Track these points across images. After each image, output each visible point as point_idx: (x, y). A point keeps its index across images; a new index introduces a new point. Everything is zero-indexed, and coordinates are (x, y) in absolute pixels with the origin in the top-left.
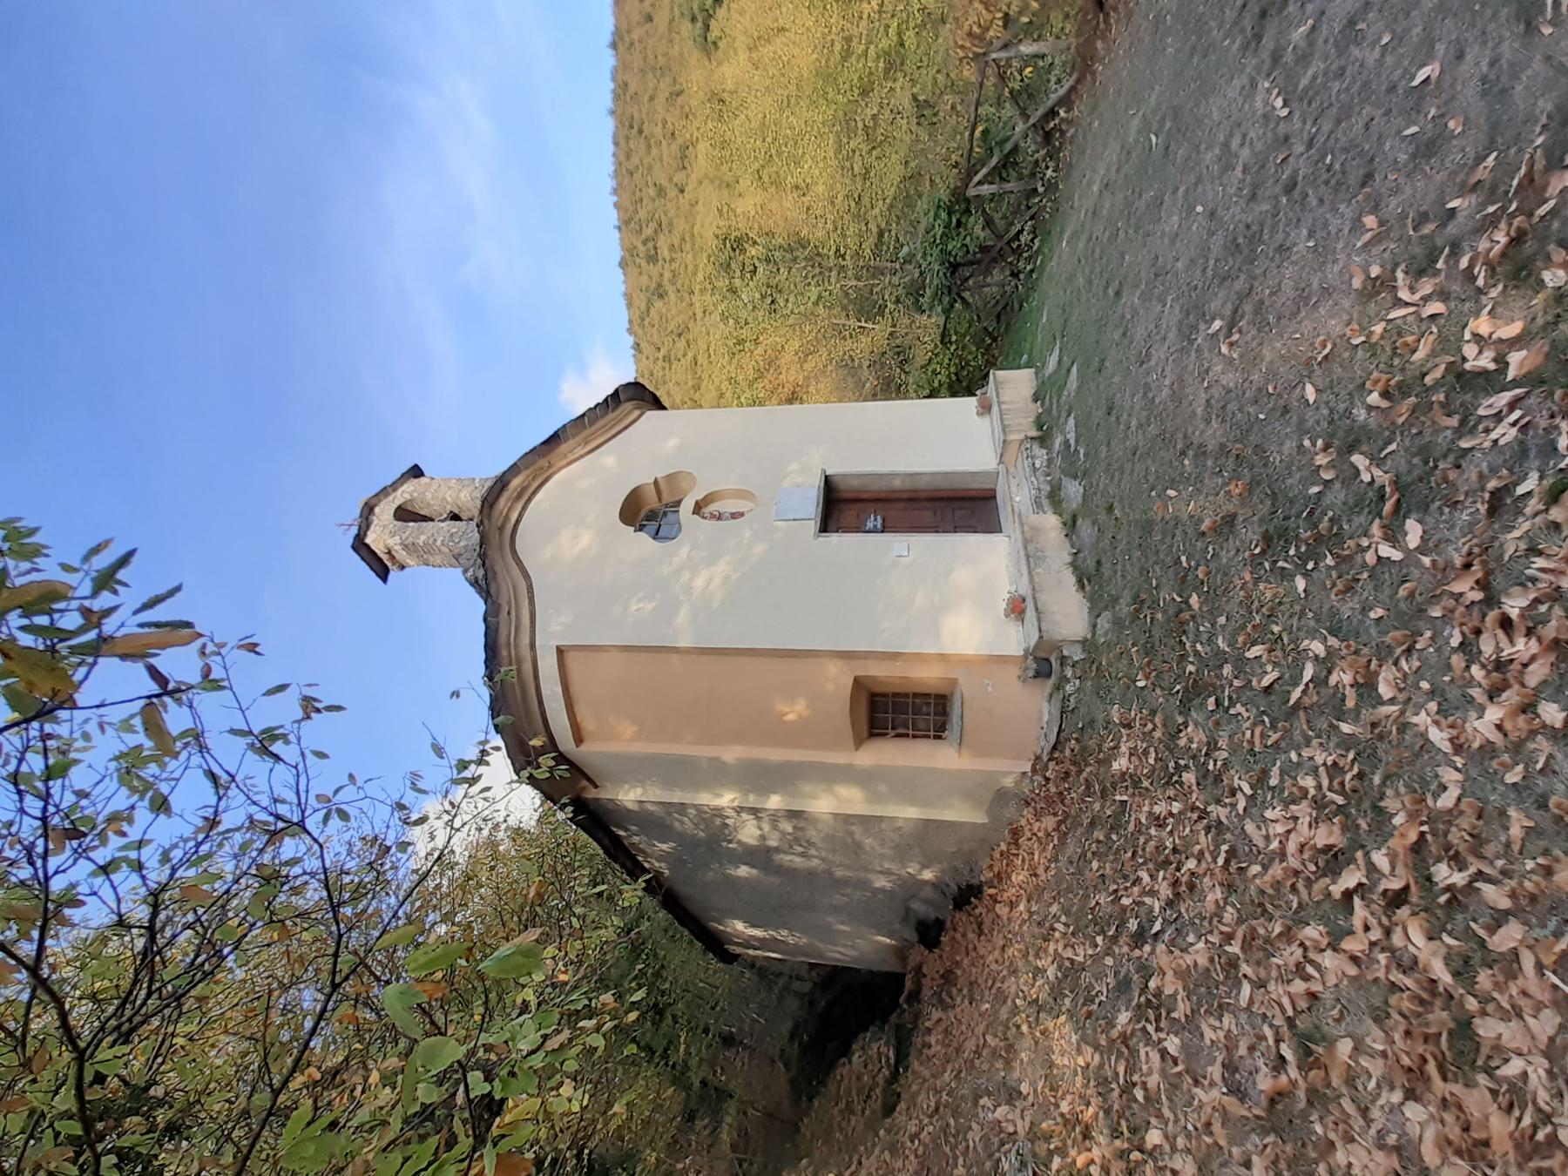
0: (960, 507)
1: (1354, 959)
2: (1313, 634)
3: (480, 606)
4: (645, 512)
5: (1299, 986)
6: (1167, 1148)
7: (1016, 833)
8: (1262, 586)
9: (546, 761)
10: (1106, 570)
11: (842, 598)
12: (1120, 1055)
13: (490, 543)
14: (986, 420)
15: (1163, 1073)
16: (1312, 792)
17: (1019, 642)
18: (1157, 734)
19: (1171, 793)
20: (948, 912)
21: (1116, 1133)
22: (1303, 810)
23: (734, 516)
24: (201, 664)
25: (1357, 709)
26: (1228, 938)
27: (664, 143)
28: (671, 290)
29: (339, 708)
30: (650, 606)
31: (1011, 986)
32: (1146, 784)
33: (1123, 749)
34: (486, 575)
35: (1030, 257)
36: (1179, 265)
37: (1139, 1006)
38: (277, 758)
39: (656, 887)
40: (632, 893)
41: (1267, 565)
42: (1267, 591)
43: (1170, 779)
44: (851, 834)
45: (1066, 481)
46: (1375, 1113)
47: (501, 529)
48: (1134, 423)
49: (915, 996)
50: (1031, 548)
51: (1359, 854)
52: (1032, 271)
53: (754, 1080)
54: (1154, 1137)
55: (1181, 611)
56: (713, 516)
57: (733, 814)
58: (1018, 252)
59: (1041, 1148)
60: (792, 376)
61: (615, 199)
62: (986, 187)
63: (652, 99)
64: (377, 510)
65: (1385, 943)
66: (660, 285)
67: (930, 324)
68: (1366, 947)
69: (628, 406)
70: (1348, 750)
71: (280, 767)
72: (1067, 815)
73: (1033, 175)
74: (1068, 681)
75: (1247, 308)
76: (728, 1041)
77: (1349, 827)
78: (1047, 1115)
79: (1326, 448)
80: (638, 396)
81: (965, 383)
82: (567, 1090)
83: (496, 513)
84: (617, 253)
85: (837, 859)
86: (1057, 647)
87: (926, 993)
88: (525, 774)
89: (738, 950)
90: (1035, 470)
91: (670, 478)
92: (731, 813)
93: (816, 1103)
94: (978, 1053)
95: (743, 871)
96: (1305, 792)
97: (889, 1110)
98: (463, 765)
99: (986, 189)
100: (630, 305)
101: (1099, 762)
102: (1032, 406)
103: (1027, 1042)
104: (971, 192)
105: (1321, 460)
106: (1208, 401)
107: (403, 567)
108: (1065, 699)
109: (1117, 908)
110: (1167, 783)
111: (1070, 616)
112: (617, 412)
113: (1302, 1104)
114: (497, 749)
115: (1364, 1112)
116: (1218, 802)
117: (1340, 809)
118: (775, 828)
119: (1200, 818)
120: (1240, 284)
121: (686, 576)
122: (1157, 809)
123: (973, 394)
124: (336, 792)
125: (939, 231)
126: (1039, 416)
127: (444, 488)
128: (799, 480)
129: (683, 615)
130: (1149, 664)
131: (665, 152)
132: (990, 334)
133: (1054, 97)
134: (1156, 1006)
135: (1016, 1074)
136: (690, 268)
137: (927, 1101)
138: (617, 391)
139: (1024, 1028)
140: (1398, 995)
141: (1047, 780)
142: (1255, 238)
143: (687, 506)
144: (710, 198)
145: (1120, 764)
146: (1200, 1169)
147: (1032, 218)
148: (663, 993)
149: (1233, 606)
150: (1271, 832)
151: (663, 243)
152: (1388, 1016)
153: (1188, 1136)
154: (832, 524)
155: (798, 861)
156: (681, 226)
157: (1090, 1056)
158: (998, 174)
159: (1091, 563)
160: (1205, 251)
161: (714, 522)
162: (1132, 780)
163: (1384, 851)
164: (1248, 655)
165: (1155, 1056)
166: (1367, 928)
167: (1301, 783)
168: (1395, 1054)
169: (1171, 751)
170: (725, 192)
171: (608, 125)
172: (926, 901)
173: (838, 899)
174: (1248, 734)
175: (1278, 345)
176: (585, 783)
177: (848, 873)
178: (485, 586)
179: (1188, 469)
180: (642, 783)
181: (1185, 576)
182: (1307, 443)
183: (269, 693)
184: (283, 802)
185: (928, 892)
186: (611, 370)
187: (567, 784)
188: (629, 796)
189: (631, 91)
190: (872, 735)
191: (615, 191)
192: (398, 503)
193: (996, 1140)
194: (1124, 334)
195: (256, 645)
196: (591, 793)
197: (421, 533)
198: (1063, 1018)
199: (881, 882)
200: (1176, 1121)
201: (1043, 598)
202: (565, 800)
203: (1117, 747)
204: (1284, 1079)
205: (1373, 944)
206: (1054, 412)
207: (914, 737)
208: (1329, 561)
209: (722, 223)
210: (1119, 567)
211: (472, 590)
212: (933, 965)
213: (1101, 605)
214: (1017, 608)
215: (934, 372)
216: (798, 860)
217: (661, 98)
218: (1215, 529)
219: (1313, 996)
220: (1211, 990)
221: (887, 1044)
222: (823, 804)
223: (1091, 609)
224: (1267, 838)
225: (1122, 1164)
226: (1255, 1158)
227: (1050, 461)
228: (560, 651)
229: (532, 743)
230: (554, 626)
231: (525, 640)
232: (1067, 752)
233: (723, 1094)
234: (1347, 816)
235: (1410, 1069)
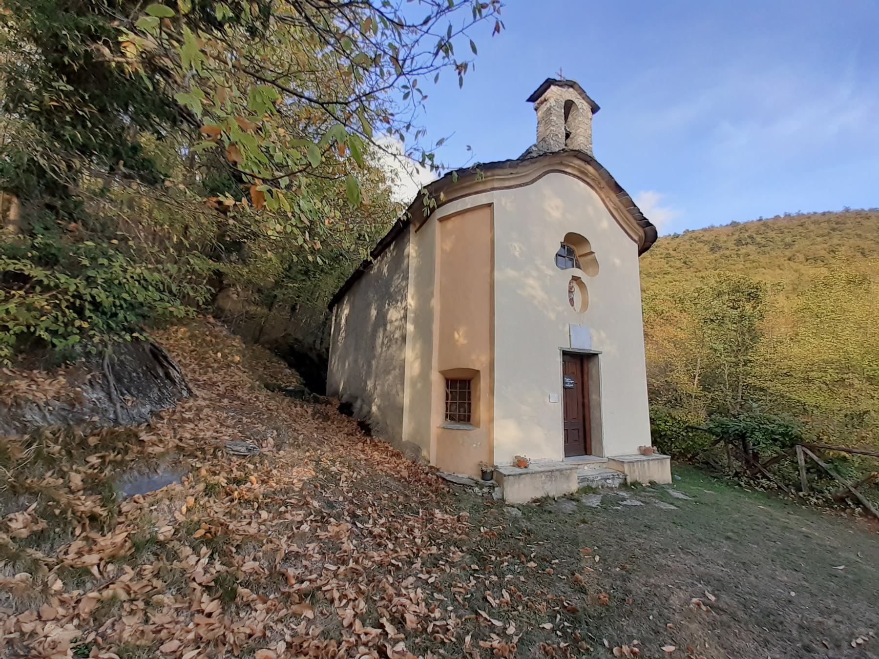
0: (580, 435)
1: (351, 625)
2: (519, 628)
3: (515, 157)
4: (573, 249)
5: (336, 595)
6: (260, 521)
7: (398, 455)
8: (544, 603)
9: (433, 203)
10: (546, 516)
11: (534, 364)
12: (299, 501)
13: (541, 160)
14: (637, 452)
15: (292, 521)
16: (432, 615)
17: (501, 463)
18: (455, 535)
19: (426, 539)
20: (357, 419)
21: (265, 496)
22: (423, 609)
23: (572, 301)
24: (487, 2)
25: (479, 647)
26: (356, 561)
27: (825, 246)
28: (717, 255)
29: (461, 85)
30: (517, 254)
31: (326, 448)
32: (429, 526)
33: (446, 516)
34: (533, 158)
35: (750, 485)
36: (752, 578)
37: (322, 512)
38: (436, 54)
39: (367, 264)
40: (364, 254)
41: (557, 608)
42: (542, 606)
43: (432, 539)
44: (394, 369)
45: (599, 497)
46: (280, 626)
47: (561, 163)
48: (641, 541)
49: (316, 401)
50: (557, 473)
51: (402, 636)
52: (740, 485)
53: (277, 322)
54: (264, 514)
55: (526, 556)
56: (571, 288)
57: (404, 305)
58: (754, 477)
59: (257, 459)
60: (659, 333)
61: (782, 216)
62: (803, 458)
63: (859, 236)
64: (571, 89)
65: (359, 642)
66: (720, 248)
67: (698, 417)
68: (357, 632)
69: (641, 232)
70: (456, 638)
71: (431, 57)
72: (409, 482)
73: (812, 489)
74: (481, 489)
75: (725, 618)
76: (293, 308)
77: (416, 633)
78: (271, 463)
79: (632, 652)
80: (647, 238)
81: (661, 440)
82: (279, 228)
84: (741, 219)
85: (382, 362)
86: (500, 484)
87: (318, 406)
88: (426, 191)
89: (334, 311)
90: (606, 479)
92: (404, 304)
93: (268, 351)
94: (295, 430)
95: (374, 312)
96: (432, 611)
97: (267, 386)
98: (431, 157)
99: (801, 459)
100: (705, 230)
101: (438, 502)
102: (647, 480)
103: (302, 456)
104: (799, 449)
105: (625, 649)
106: (659, 586)
107: (536, 110)
108: (471, 487)
109: (366, 505)
110: (430, 538)
111: (519, 493)
113: (282, 590)
114: (439, 175)
115: (280, 620)
116: (423, 564)
117: (425, 630)
118: (396, 328)
119: (414, 553)
120: (740, 614)
121: (535, 274)
122: (416, 530)
123: (654, 443)
124: (419, 90)
125: (770, 427)
126: (640, 484)
127: (585, 127)
128: (595, 338)
129: (511, 273)
130: (493, 534)
131: (818, 247)
132: (693, 457)
133: (869, 505)
134: (323, 521)
135: (287, 449)
136: (733, 267)
137: (273, 404)
138: (652, 225)
139: (308, 454)
140: (336, 646)
141: (427, 474)
142: (774, 627)
143: (577, 272)
144: (787, 277)
145: (438, 514)
146: (252, 536)
147: (779, 487)
148: (314, 274)
149: (530, 586)
150: (410, 590)
151: (751, 248)
152: (325, 639)
153: (266, 532)
154: (567, 357)
155: (379, 341)
156: (763, 260)
157: (298, 486)
158: (812, 467)
159: (549, 507)
160: (766, 596)
161: (568, 289)
162: (431, 519)
163: (405, 649)
164: (504, 591)
165: (299, 518)
166: (366, 634)
167: (437, 610)
168: (308, 640)
169: (447, 541)
170: (790, 288)
171: (837, 208)
172: (361, 408)
173: (361, 362)
174: (460, 585)
175: (700, 633)
176: (418, 226)
177: (374, 367)
178: (527, 158)
179: (613, 570)
180: (418, 256)
181: (546, 560)
182: (635, 642)
183: (472, 43)
184: (412, 62)
185: (366, 409)
186: (665, 221)
187: (419, 213)
188: (411, 249)
189: (864, 222)
190: (447, 380)
191: (788, 216)
193: (258, 438)
194: (700, 540)
195: (498, 31)
196: (412, 229)
197: (557, 118)
198: (314, 473)
199: (370, 384)
200: (272, 526)
201: (528, 478)
202: (410, 215)
203: (447, 513)
204: (293, 581)
205: (359, 636)
206: (643, 493)
207: (447, 403)
208: (562, 645)
209: (769, 286)
210: (548, 524)
211: (524, 151)
212: (332, 410)
213: (526, 511)
214: (521, 463)
215: (666, 422)
216: (380, 341)
217: (859, 242)
218: (577, 581)
219: (332, 601)
220: (330, 548)
221: (295, 387)
222: (410, 354)
223: (522, 505)
224: (406, 588)
225: (252, 498)
226: (257, 563)
227: (612, 489)
228: (490, 205)
229: (442, 194)
230: (504, 200)
231: (496, 185)
232: (442, 486)
233: (270, 307)
234: (422, 633)
235: (301, 647)
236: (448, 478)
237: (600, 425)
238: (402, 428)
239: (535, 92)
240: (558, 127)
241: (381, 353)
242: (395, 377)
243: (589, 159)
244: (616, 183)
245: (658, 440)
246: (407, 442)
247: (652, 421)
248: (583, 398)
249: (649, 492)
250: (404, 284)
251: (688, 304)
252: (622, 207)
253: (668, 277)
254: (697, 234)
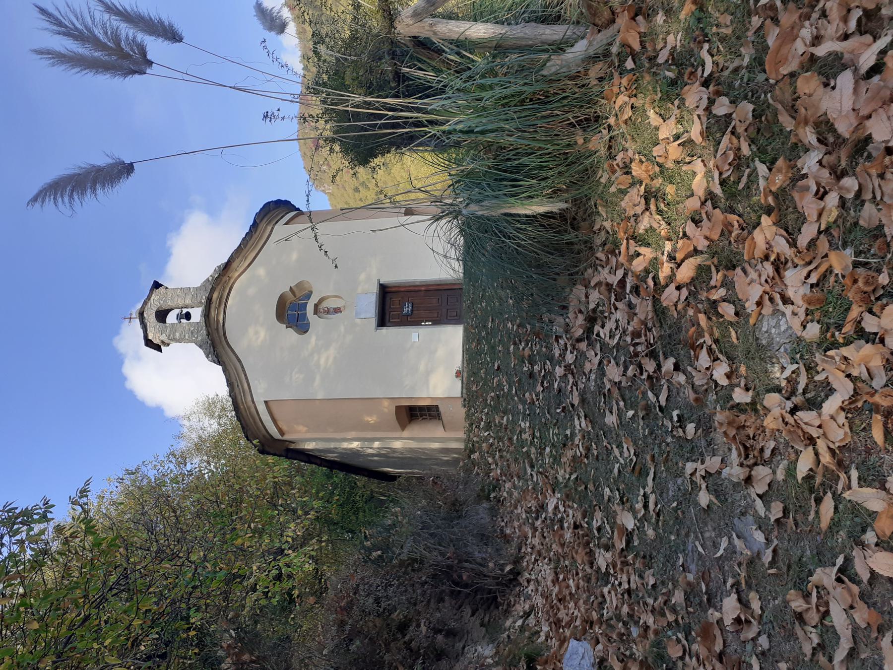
23: (337, 310)
47: (217, 329)
56: (328, 312)
83: (212, 322)
91: (300, 285)
112: (257, 233)
121: (316, 357)
138: (255, 221)
143: (310, 308)
228: (266, 402)
230: (261, 391)
231: (249, 399)
252: (243, 254)
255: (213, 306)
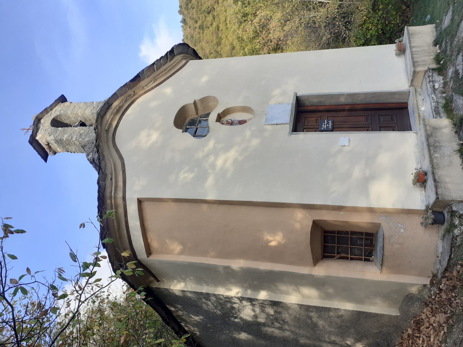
0: (385, 114)
3: (95, 175)
4: (190, 120)
7: (418, 323)
13: (103, 152)
23: (241, 122)
29: (23, 232)
44: (311, 318)
47: (107, 131)
50: (431, 140)
57: (237, 301)
60: (276, 34)
64: (42, 121)
74: (456, 227)
80: (185, 52)
81: (388, 34)
85: (302, 332)
86: (448, 204)
90: (434, 89)
92: (237, 301)
95: (243, 336)
98: (86, 266)
102: (432, 48)
107: (55, 153)
112: (172, 62)
118: (263, 311)
121: (212, 158)
123: (392, 42)
124: (21, 278)
138: (173, 49)
141: (441, 290)
143: (213, 117)
155: (277, 332)
161: (228, 127)
176: (152, 278)
178: (98, 164)
180: (184, 280)
188: (177, 287)
192: (53, 117)
196: (155, 285)
197: (64, 134)
201: (440, 173)
202: (141, 288)
206: (448, 52)
207: (352, 259)
211: (91, 166)
214: (421, 179)
215: (367, 29)
222: (293, 298)
227: (445, 84)
228: (140, 202)
230: (136, 187)
231: (120, 195)
232: (455, 273)
236: (445, 264)
237: (374, 94)
238: (382, 316)
239: (39, 154)
240: (74, 133)
241: (292, 332)
242: (319, 317)
243: (107, 106)
244: (132, 81)
245: (387, 36)
246: (401, 309)
247: (366, 43)
248: (343, 110)
249: (446, 47)
250: (213, 298)
251: (248, 10)
252: (154, 75)
253: (222, 26)
254: (183, 4)
255: (110, 111)
